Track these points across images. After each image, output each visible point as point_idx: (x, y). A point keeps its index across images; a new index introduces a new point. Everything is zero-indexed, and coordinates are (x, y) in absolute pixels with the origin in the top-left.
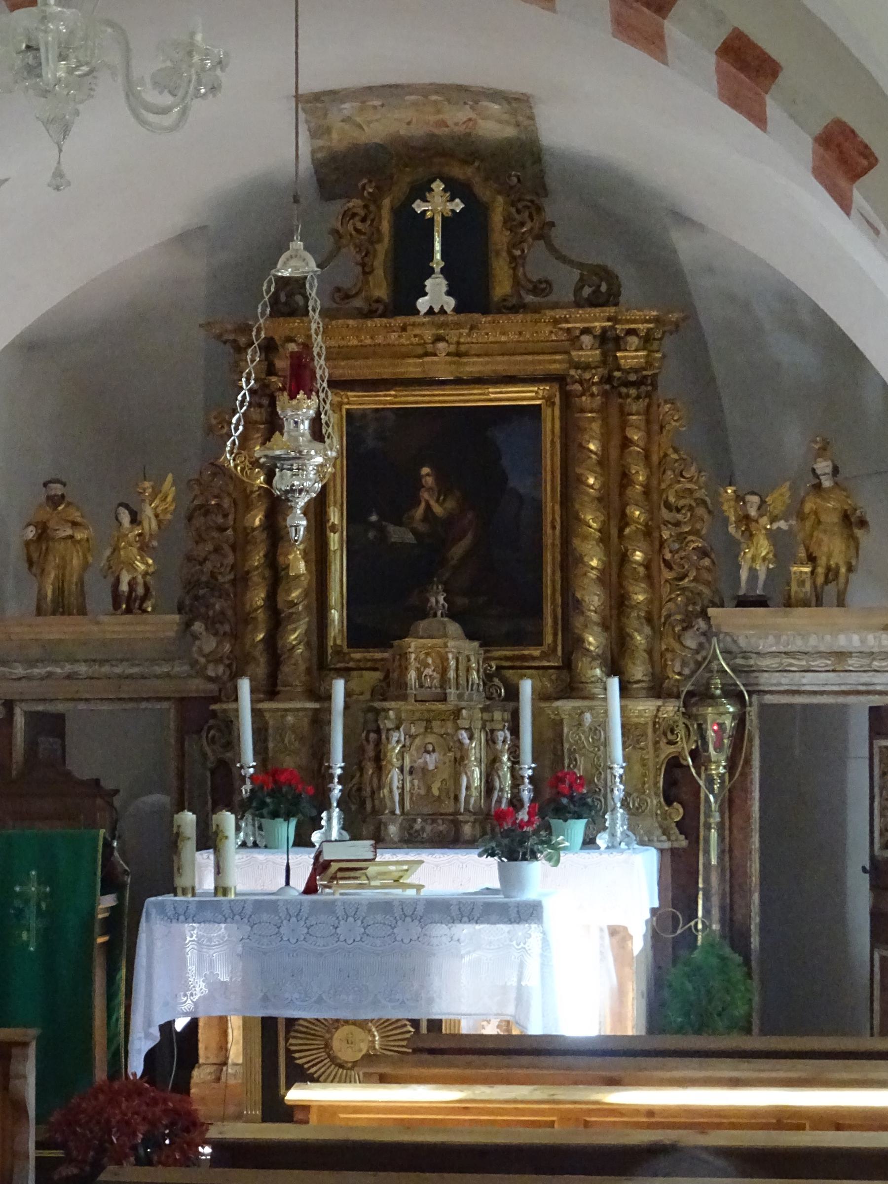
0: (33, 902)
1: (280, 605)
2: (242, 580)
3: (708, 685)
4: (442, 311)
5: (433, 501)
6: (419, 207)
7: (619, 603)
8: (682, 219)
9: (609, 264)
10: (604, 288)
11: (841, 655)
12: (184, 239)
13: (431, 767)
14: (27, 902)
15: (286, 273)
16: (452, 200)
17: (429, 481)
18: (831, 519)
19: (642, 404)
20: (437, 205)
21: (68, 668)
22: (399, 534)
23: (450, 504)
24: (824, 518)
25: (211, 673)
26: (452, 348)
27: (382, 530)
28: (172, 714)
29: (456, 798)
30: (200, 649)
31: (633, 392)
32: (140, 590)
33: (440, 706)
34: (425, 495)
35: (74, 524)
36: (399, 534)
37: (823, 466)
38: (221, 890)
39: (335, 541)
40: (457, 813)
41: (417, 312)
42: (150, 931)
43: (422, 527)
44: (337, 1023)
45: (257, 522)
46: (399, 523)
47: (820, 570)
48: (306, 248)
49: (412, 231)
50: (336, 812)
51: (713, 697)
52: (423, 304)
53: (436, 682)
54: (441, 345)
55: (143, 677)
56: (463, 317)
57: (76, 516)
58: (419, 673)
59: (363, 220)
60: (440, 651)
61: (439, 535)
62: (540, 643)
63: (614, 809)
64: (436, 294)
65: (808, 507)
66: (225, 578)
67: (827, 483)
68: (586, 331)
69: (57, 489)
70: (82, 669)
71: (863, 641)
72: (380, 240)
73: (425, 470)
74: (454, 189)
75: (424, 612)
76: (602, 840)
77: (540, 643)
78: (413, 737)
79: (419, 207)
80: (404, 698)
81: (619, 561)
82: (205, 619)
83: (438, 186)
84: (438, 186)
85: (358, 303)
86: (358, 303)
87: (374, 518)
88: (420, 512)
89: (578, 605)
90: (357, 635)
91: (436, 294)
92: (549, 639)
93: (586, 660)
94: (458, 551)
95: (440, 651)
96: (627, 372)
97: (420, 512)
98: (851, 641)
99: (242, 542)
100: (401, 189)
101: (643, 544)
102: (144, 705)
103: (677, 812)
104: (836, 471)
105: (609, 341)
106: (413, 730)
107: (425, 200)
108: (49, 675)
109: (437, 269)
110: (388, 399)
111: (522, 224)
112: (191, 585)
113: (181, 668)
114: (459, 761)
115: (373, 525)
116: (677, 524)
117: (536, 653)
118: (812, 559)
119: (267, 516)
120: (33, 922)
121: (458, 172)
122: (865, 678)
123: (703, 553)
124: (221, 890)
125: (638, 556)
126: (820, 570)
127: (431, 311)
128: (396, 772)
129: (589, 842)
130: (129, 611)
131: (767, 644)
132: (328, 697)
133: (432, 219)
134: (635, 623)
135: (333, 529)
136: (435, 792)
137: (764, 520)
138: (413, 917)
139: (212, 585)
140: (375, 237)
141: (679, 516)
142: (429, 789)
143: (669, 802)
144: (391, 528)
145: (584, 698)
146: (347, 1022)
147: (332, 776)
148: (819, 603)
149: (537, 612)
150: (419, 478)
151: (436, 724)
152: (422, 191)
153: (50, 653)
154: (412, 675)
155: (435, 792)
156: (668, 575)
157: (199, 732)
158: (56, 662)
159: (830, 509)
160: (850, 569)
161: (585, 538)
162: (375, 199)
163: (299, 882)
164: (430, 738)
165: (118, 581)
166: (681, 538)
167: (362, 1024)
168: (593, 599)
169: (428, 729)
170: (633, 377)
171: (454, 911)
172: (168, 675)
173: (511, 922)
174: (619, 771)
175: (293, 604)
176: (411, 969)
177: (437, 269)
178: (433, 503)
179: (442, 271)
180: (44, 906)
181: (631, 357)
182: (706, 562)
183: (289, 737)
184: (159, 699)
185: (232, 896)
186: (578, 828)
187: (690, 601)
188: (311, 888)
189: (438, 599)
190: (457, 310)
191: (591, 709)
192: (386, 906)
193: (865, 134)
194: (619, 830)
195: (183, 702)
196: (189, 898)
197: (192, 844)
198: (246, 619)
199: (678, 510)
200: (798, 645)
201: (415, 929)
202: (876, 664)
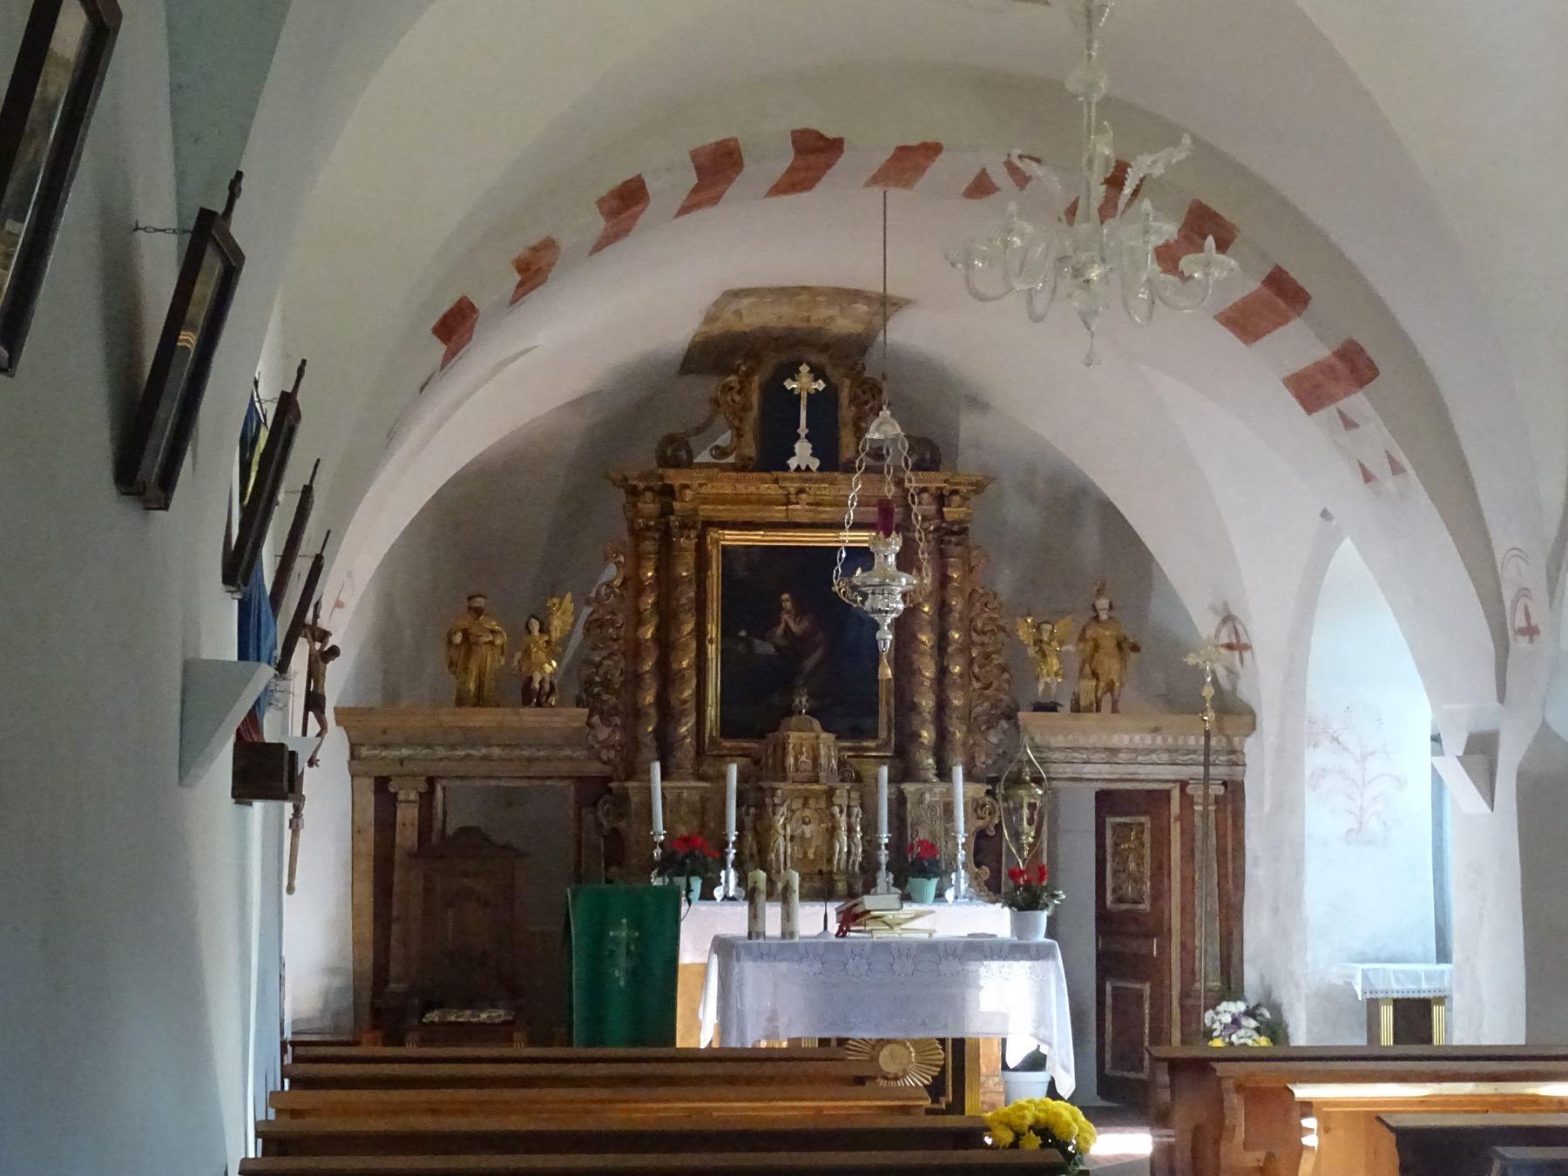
0: (623, 946)
1: (673, 700)
2: (634, 680)
3: (1020, 771)
4: (808, 469)
5: (791, 621)
6: (790, 385)
7: (942, 706)
8: (977, 403)
9: (666, 432)
10: (928, 456)
11: (1114, 751)
12: (577, 404)
13: (808, 835)
14: (618, 945)
15: (876, 436)
16: (816, 380)
17: (788, 605)
18: (1109, 644)
19: (959, 550)
20: (804, 384)
21: (484, 751)
22: (765, 648)
23: (805, 624)
24: (1103, 642)
25: (604, 756)
26: (810, 499)
27: (749, 645)
28: (572, 788)
29: (830, 861)
30: (595, 737)
31: (953, 539)
32: (547, 687)
33: (816, 787)
34: (785, 617)
35: (492, 631)
36: (765, 648)
37: (1103, 603)
38: (788, 933)
39: (712, 651)
40: (831, 873)
41: (787, 468)
42: (741, 972)
43: (782, 642)
44: (882, 1043)
45: (649, 635)
46: (763, 638)
47: (1102, 684)
48: (893, 415)
49: (779, 406)
50: (732, 874)
51: (1025, 782)
52: (793, 463)
53: (809, 767)
54: (803, 496)
55: (548, 760)
56: (826, 475)
57: (494, 624)
58: (796, 759)
59: (739, 392)
60: (809, 742)
61: (795, 648)
62: (875, 737)
63: (956, 870)
64: (803, 453)
65: (1089, 633)
66: (617, 679)
67: (1104, 616)
68: (924, 490)
69: (479, 602)
70: (496, 751)
71: (1165, 740)
72: (750, 409)
73: (785, 596)
74: (817, 373)
75: (790, 711)
76: (950, 894)
77: (875, 737)
78: (793, 812)
79: (790, 385)
80: (784, 779)
81: (942, 671)
82: (601, 714)
83: (804, 369)
84: (804, 369)
85: (731, 459)
86: (731, 459)
87: (743, 633)
88: (780, 630)
89: (914, 708)
90: (729, 728)
91: (803, 453)
92: (883, 734)
93: (923, 752)
94: (810, 663)
95: (809, 742)
96: (953, 523)
97: (780, 630)
98: (1120, 740)
99: (635, 651)
100: (767, 370)
101: (960, 660)
102: (549, 783)
103: (986, 871)
104: (1111, 607)
105: (941, 499)
106: (794, 806)
107: (794, 380)
108: (468, 756)
109: (803, 435)
110: (757, 538)
111: (866, 403)
112: (588, 684)
113: (580, 753)
114: (832, 832)
115: (741, 638)
116: (983, 645)
117: (872, 744)
118: (1095, 675)
119: (657, 629)
120: (622, 960)
121: (815, 358)
122: (1132, 768)
123: (1003, 669)
124: (788, 933)
125: (957, 669)
126: (1102, 684)
127: (798, 469)
128: (781, 839)
129: (707, 895)
130: (539, 705)
131: (1059, 741)
132: (723, 777)
133: (799, 396)
134: (955, 721)
135: (711, 641)
136: (811, 856)
137: (1054, 644)
138: (955, 956)
139: (607, 685)
140: (746, 408)
141: (986, 639)
142: (805, 853)
143: (978, 865)
144: (757, 641)
145: (918, 781)
146: (889, 1041)
147: (879, 846)
148: (1098, 710)
149: (875, 713)
150: (780, 602)
151: (812, 803)
152: (793, 373)
153: (471, 737)
154: (791, 761)
155: (811, 856)
156: (976, 685)
157: (595, 804)
158: (473, 746)
159: (1107, 636)
160: (1122, 685)
161: (923, 653)
162: (749, 374)
163: (834, 927)
164: (807, 813)
165: (531, 679)
166: (987, 656)
167: (902, 1043)
168: (927, 703)
169: (805, 804)
170: (956, 528)
171: (1033, 953)
172: (570, 759)
173: (1031, 959)
174: (961, 840)
175: (685, 702)
176: (954, 995)
177: (803, 435)
178: (791, 624)
179: (807, 436)
180: (633, 948)
181: (951, 513)
182: (1006, 676)
183: (684, 809)
184: (561, 778)
185: (797, 939)
186: (932, 885)
187: (994, 706)
188: (842, 933)
189: (802, 701)
190: (819, 469)
191: (931, 790)
192: (885, 946)
193: (1371, 352)
194: (963, 886)
195: (581, 780)
196: (761, 940)
197: (763, 897)
198: (637, 714)
199: (984, 633)
200: (1082, 741)
201: (956, 965)
202: (1140, 758)
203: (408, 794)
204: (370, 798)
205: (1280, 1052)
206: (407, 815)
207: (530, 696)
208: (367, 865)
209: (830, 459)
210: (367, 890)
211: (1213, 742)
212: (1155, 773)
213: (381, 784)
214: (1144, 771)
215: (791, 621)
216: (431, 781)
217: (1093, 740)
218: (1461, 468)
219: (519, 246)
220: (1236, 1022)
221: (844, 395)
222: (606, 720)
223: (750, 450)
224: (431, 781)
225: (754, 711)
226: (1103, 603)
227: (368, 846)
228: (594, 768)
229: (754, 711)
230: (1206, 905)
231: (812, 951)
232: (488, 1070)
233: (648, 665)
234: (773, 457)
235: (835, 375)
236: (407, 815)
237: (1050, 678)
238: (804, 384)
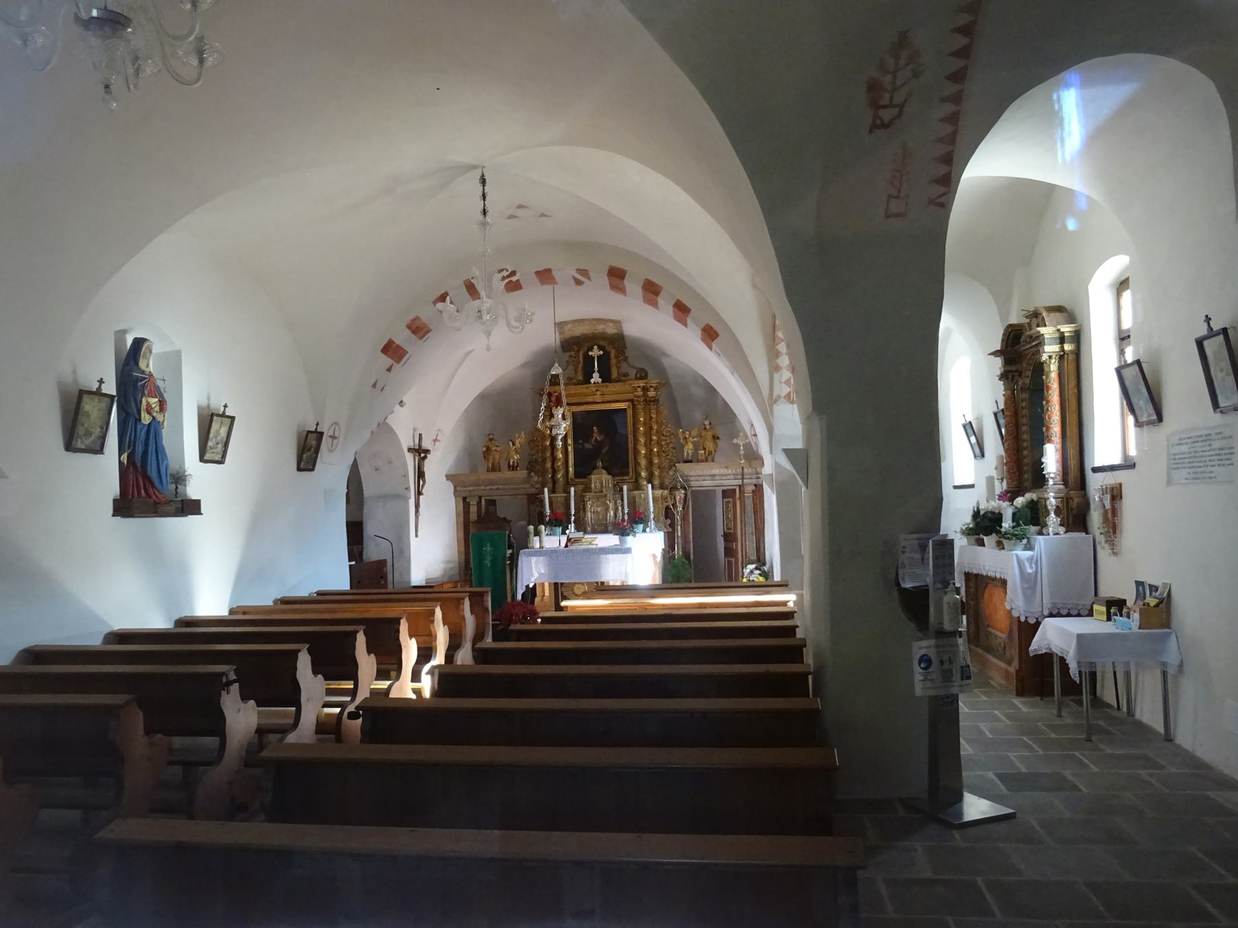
2: (544, 460)
5: (597, 436)
7: (650, 463)
8: (665, 354)
12: (525, 365)
22: (587, 446)
36: (587, 446)
37: (707, 423)
38: (541, 547)
49: (589, 361)
52: (592, 381)
61: (599, 445)
64: (596, 378)
74: (600, 348)
75: (595, 468)
90: (577, 475)
91: (596, 378)
94: (604, 451)
95: (601, 478)
100: (585, 349)
103: (669, 521)
112: (530, 462)
114: (607, 509)
121: (602, 343)
124: (541, 547)
129: (644, 531)
131: (693, 473)
149: (628, 467)
152: (591, 349)
153: (492, 483)
162: (578, 351)
168: (643, 462)
181: (651, 393)
186: (641, 526)
192: (587, 551)
203: (473, 502)
204: (461, 505)
205: (769, 583)
206: (473, 509)
207: (512, 468)
208: (462, 527)
209: (606, 378)
210: (462, 535)
211: (746, 470)
212: (732, 483)
213: (464, 499)
214: (705, 483)
215: (597, 436)
216: (480, 498)
217: (706, 472)
218: (748, 365)
219: (687, 302)
220: (752, 572)
221: (612, 355)
222: (536, 473)
223: (581, 378)
224: (480, 498)
225: (584, 468)
226: (707, 423)
227: (462, 520)
228: (533, 491)
229: (584, 468)
230: (750, 529)
231: (552, 553)
232: (375, 597)
233: (548, 454)
234: (587, 379)
235: (609, 349)
236: (473, 509)
237: (689, 449)
238: (596, 352)
